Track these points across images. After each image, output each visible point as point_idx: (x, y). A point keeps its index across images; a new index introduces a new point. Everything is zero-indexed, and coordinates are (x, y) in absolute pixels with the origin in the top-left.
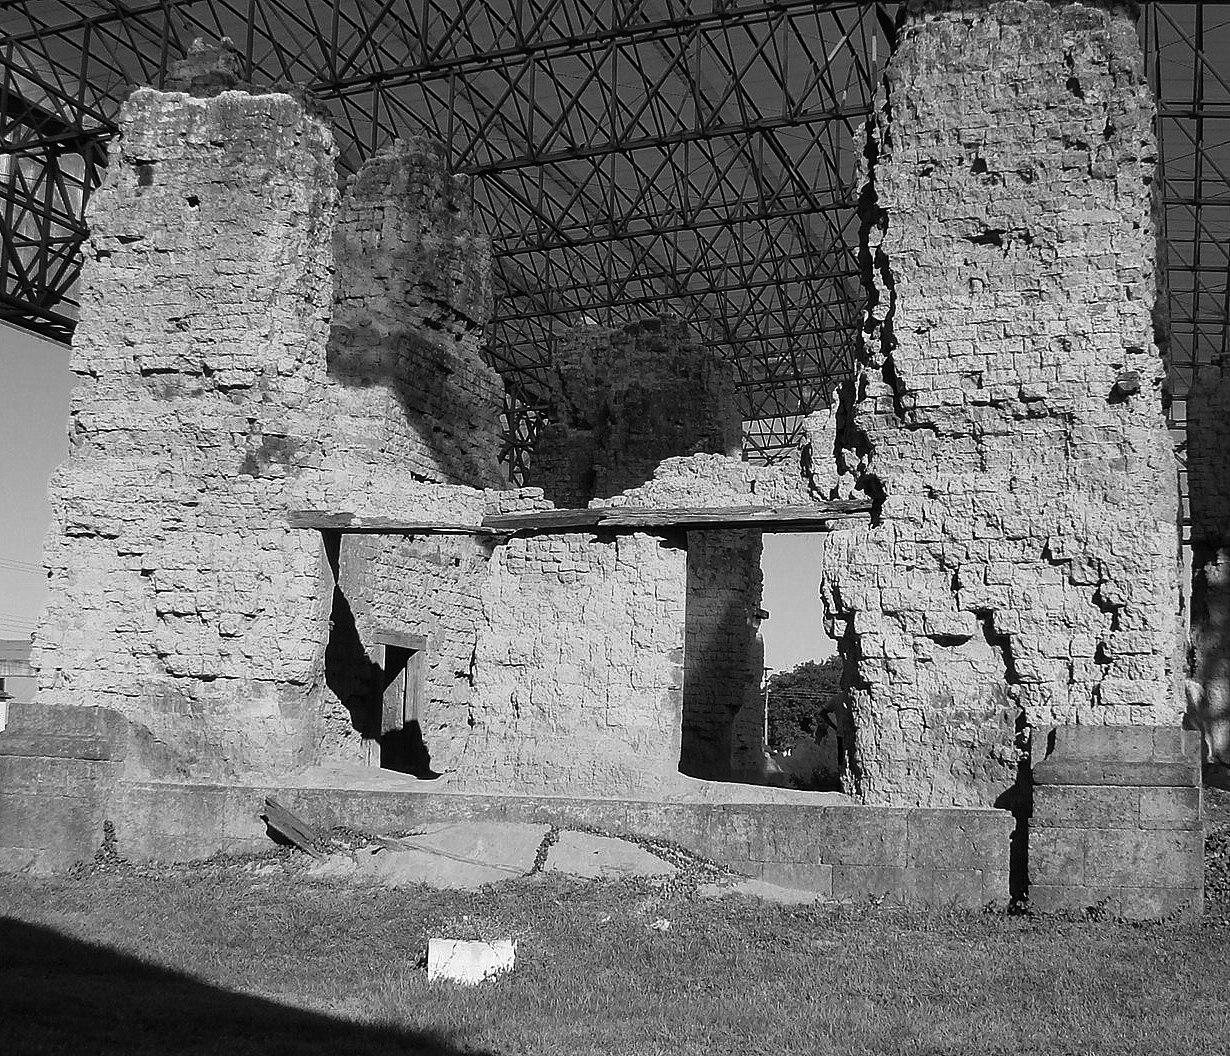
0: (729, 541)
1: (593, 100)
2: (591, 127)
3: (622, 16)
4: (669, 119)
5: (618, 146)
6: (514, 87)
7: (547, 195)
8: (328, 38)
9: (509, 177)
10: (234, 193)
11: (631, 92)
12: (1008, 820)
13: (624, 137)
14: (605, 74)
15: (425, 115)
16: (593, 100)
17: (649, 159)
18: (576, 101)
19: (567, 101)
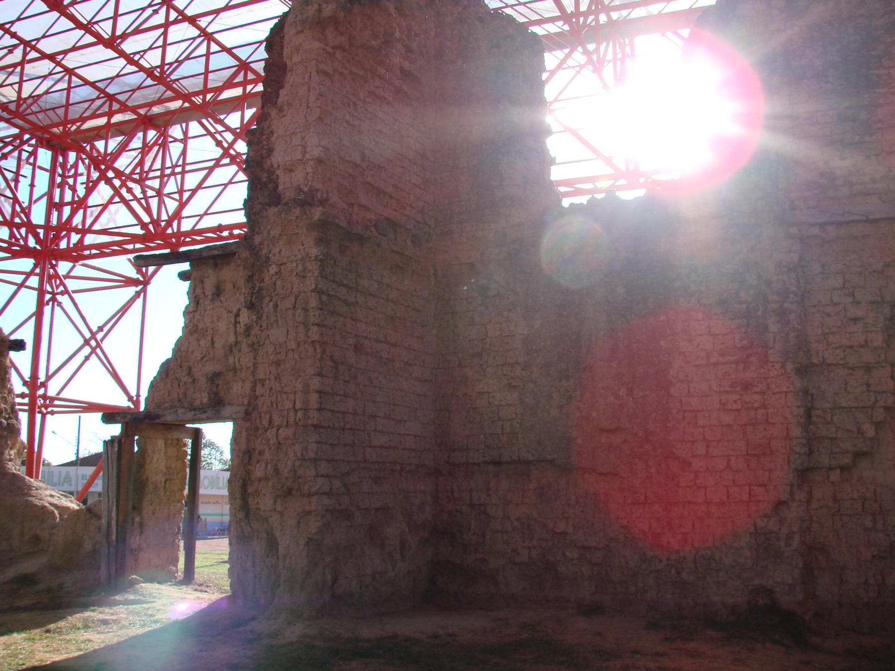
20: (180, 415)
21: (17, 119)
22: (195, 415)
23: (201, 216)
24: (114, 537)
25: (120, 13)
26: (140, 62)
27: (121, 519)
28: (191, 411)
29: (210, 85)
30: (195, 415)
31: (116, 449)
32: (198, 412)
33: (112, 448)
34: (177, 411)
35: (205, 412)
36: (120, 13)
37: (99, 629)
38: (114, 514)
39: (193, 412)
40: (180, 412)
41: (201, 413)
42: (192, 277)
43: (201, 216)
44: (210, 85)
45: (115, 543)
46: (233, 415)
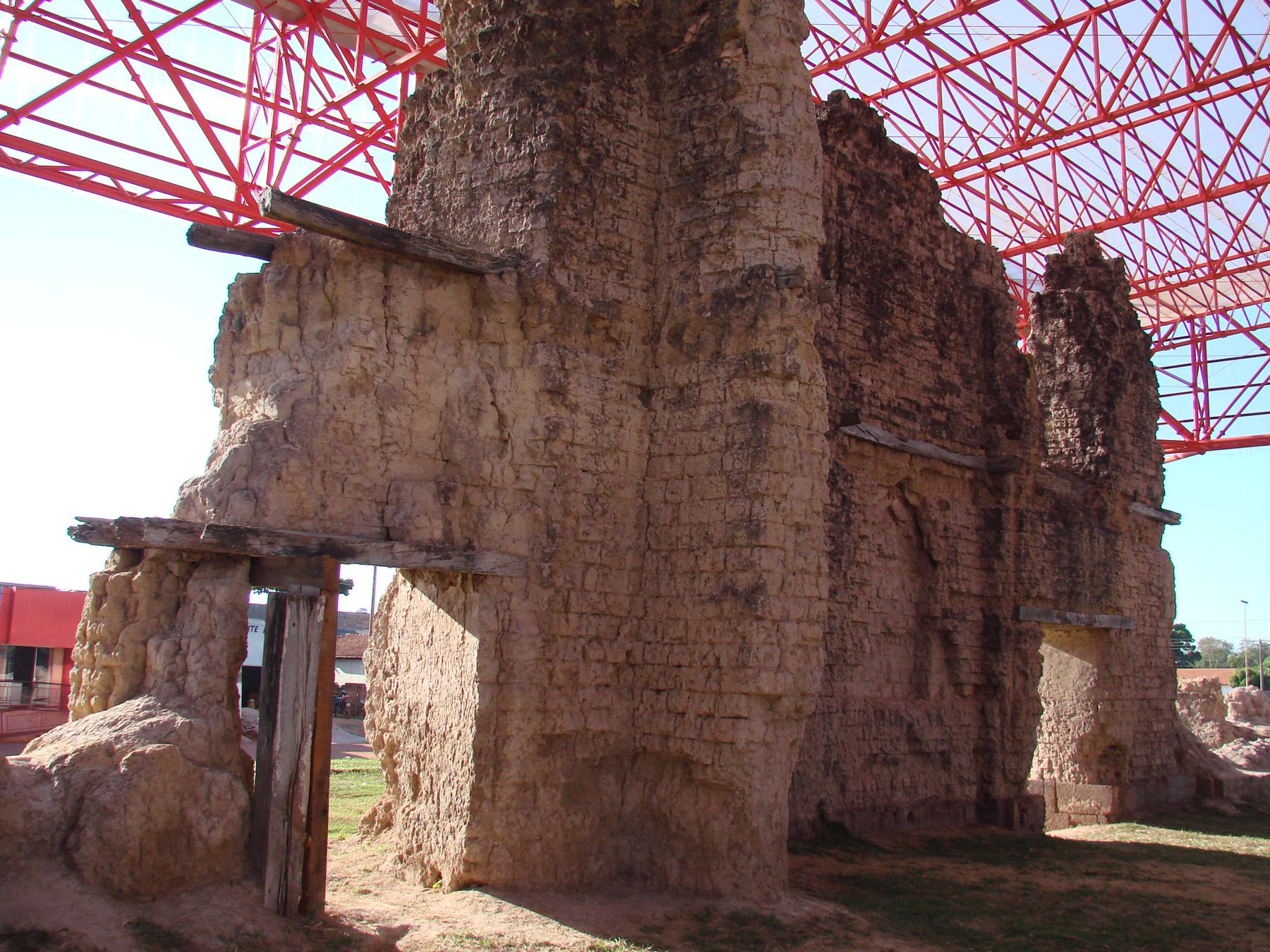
0: (477, 876)
1: (1179, 157)
2: (1180, 181)
3: (1196, 71)
4: (1253, 165)
5: (1209, 195)
6: (1075, 48)
7: (1152, 248)
8: (862, 13)
9: (1035, 24)
10: (1141, 547)
11: (1216, 146)
12: (932, 460)
13: (1212, 185)
14: (1189, 132)
15: (1030, 190)
16: (1179, 157)
17: (1239, 203)
18: (1164, 161)
19: (1133, 52)
20: (397, 555)
21: (24, 160)
22: (428, 561)
23: (157, 108)
24: (303, 809)
25: (1243, 94)
26: (1206, 92)
27: (316, 769)
28: (421, 551)
29: (1141, 58)
30: (428, 561)
31: (320, 618)
32: (433, 556)
33: (309, 615)
34: (392, 546)
35: (448, 558)
36: (1243, 94)
37: (1094, 320)
38: (306, 759)
39: (424, 554)
40: (399, 550)
41: (440, 559)
42: (279, 255)
43: (157, 108)
44: (1141, 58)
45: (304, 820)
46: (497, 570)
